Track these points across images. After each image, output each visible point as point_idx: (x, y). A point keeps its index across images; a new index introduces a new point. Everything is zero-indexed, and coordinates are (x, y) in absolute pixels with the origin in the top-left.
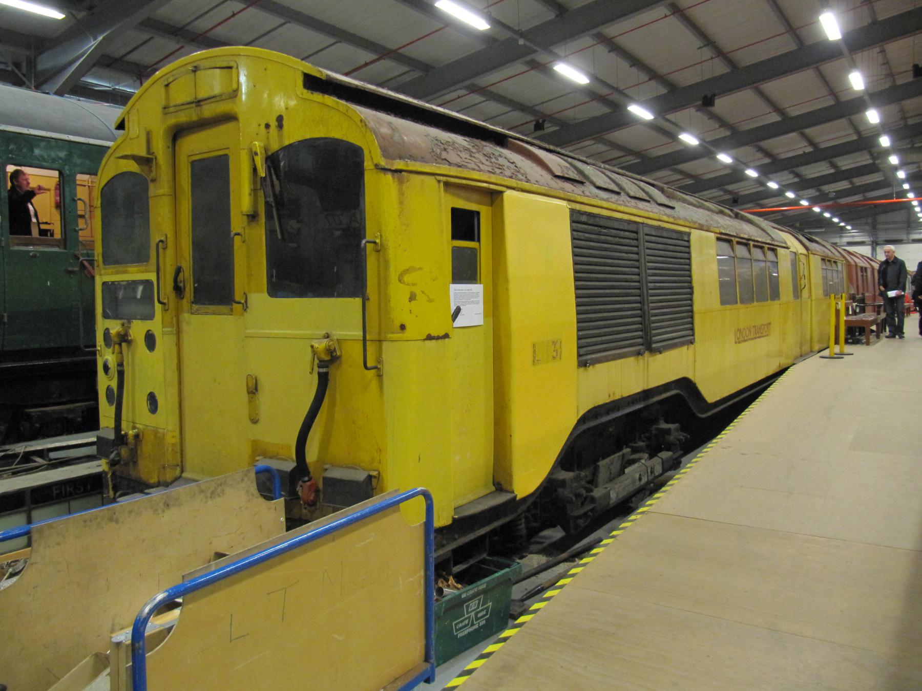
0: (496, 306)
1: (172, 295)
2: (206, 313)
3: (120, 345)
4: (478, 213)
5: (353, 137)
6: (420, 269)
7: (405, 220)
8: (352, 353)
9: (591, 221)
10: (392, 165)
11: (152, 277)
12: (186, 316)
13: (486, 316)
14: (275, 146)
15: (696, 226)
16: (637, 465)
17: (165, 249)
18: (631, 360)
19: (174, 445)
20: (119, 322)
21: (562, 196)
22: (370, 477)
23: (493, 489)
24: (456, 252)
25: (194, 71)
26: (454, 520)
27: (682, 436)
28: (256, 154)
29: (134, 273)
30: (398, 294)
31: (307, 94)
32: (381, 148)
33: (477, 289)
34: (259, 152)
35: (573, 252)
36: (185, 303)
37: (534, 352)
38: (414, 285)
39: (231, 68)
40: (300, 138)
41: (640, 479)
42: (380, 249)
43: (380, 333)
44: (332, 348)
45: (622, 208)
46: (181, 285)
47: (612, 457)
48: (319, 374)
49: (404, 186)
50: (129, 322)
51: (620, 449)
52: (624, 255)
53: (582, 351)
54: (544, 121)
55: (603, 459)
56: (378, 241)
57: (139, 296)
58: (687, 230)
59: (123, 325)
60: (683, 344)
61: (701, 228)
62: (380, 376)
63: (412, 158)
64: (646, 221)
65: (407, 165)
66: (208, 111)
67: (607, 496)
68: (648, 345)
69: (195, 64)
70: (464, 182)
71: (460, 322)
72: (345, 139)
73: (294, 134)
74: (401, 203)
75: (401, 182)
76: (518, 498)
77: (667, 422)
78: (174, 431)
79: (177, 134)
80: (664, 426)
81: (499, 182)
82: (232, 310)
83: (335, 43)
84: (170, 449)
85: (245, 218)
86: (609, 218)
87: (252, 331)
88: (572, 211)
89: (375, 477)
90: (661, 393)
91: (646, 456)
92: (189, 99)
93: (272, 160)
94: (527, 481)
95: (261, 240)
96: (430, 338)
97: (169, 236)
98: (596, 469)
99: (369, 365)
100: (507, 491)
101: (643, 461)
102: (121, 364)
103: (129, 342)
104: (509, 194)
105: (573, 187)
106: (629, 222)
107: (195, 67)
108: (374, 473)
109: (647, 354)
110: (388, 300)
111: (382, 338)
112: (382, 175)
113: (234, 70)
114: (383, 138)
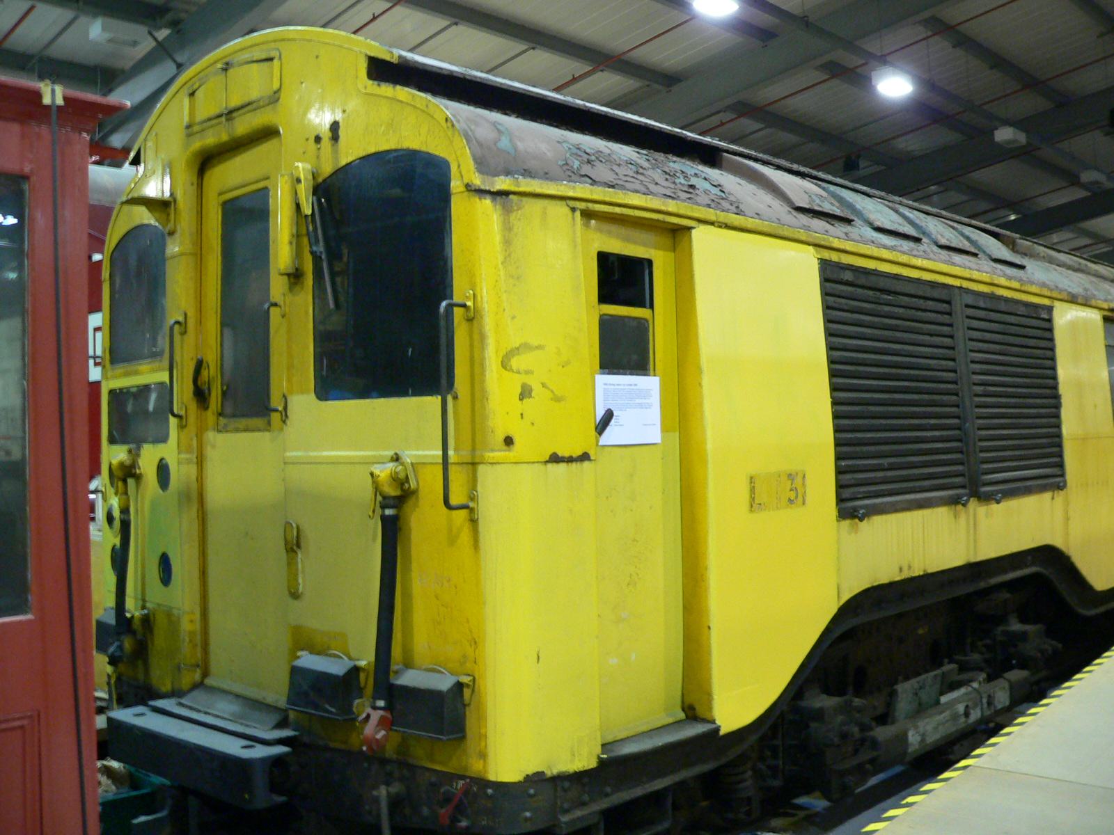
0: (681, 414)
1: (193, 406)
2: (237, 430)
3: (125, 481)
4: (650, 262)
5: (437, 147)
6: (539, 347)
7: (520, 274)
8: (429, 484)
9: (862, 280)
10: (493, 184)
11: (164, 377)
12: (211, 435)
13: (665, 429)
14: (327, 169)
15: (1064, 296)
16: (963, 690)
17: (184, 333)
18: (942, 513)
19: (192, 634)
20: (125, 448)
21: (804, 238)
22: (459, 686)
23: (682, 716)
24: (608, 327)
25: (225, 70)
26: (602, 763)
27: (1050, 645)
28: (299, 181)
29: (150, 374)
30: (500, 389)
31: (372, 86)
32: (475, 159)
33: (649, 385)
34: (302, 177)
35: (826, 329)
36: (210, 416)
37: (752, 490)
38: (528, 372)
39: (271, 59)
40: (362, 154)
41: (967, 714)
42: (473, 318)
43: (474, 450)
44: (402, 476)
45: (919, 262)
46: (205, 387)
47: (923, 677)
48: (384, 519)
49: (513, 217)
50: (139, 448)
51: (940, 665)
52: (927, 338)
53: (847, 493)
54: (859, 157)
55: (907, 678)
56: (469, 303)
57: (151, 408)
58: (1046, 302)
59: (130, 451)
60: (1043, 489)
61: (1073, 300)
62: (474, 521)
63: (528, 173)
64: (965, 284)
65: (518, 185)
66: (243, 125)
67: (902, 738)
68: (969, 485)
69: (226, 60)
70: (617, 210)
71: (612, 435)
72: (424, 149)
73: (351, 150)
74: (507, 242)
75: (507, 210)
76: (722, 732)
77: (1023, 621)
78: (192, 613)
79: (205, 162)
80: (1016, 626)
81: (682, 212)
82: (269, 423)
83: (526, 51)
84: (187, 639)
85: (286, 278)
86: (897, 277)
87: (294, 454)
88: (825, 265)
89: (468, 686)
90: (1005, 572)
91: (982, 676)
92: (217, 111)
93: (322, 189)
94: (738, 705)
95: (307, 312)
96: (555, 459)
97: (189, 314)
98: (893, 694)
99: (454, 501)
100: (704, 721)
101: (975, 685)
102: (125, 511)
103: (138, 478)
104: (700, 235)
105: (828, 226)
106: (933, 285)
107: (227, 64)
108: (465, 679)
109: (973, 503)
110: (485, 397)
111: (477, 460)
112: (476, 199)
113: (276, 62)
114: (480, 144)
